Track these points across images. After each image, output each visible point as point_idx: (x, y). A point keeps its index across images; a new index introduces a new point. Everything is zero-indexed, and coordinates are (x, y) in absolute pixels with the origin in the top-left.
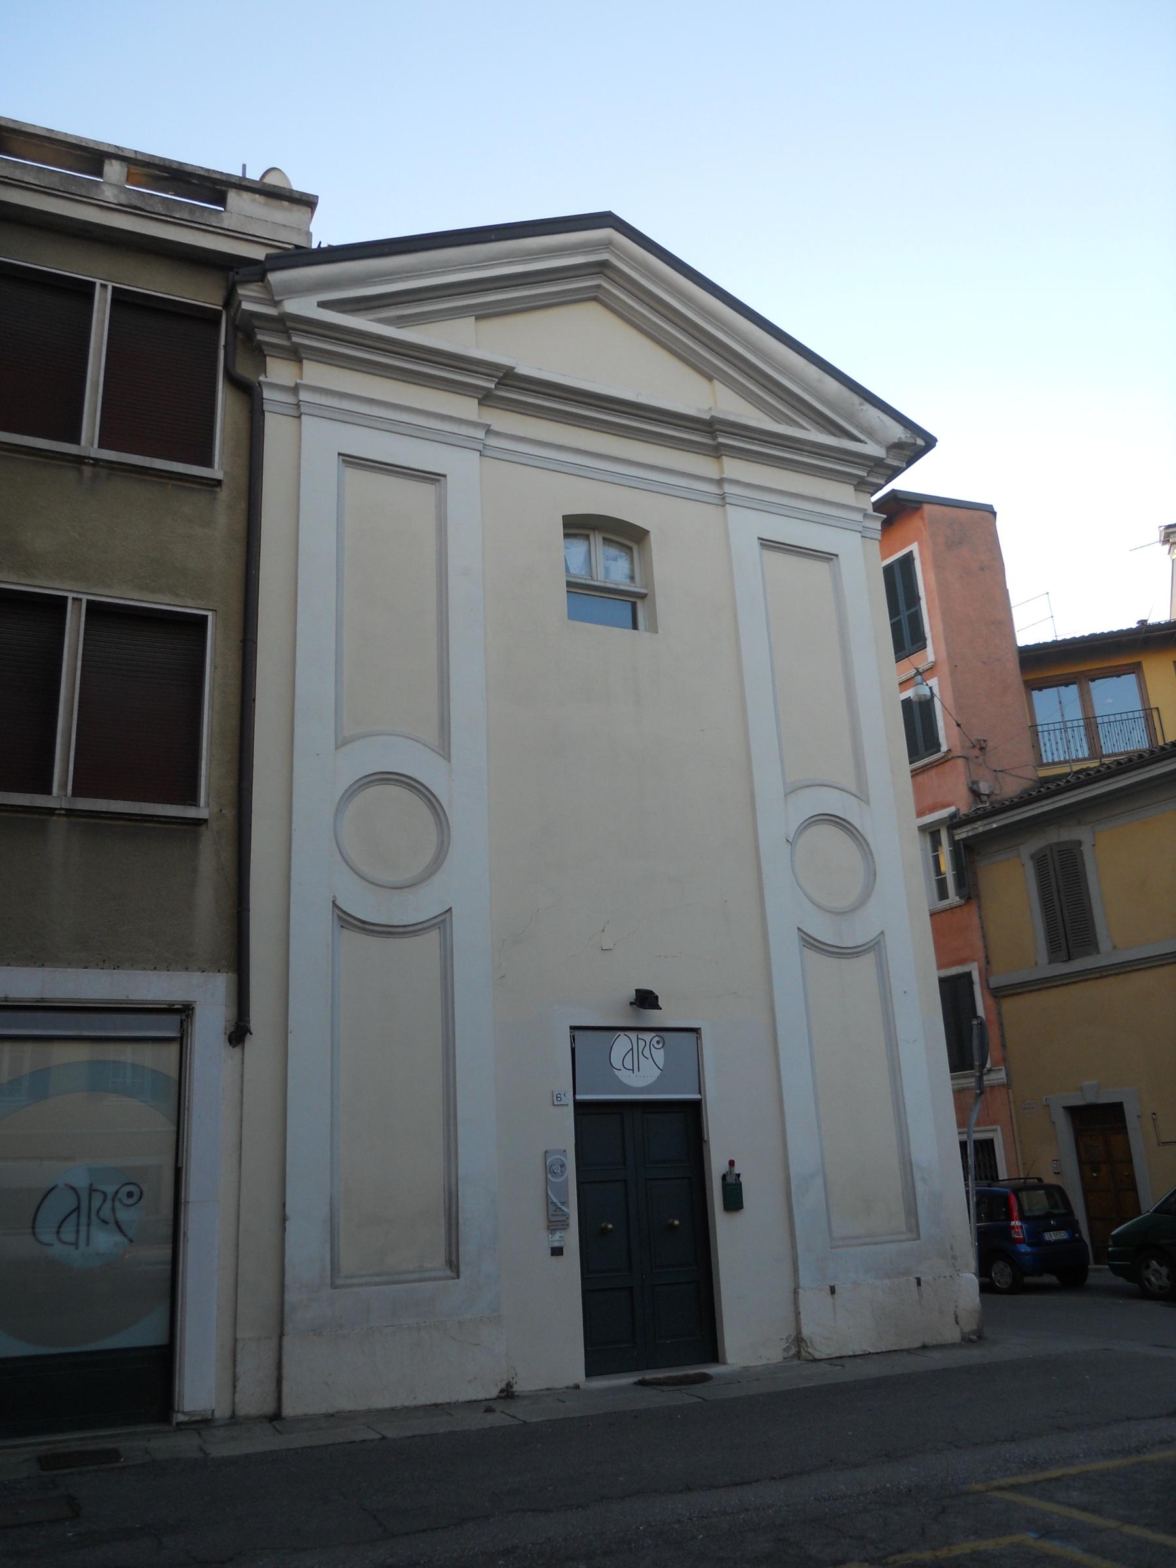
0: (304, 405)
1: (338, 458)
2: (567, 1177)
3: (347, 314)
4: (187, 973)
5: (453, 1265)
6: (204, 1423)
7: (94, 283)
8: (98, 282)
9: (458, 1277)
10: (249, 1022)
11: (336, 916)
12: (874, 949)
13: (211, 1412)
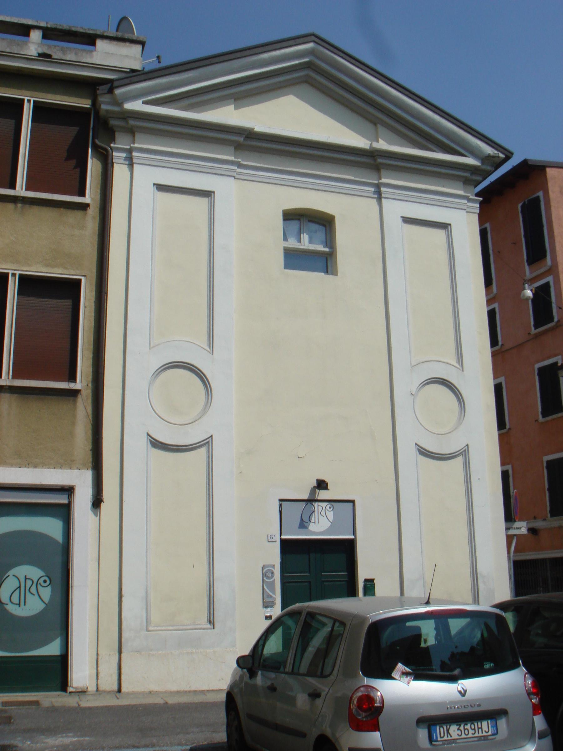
0: (135, 158)
1: (154, 186)
2: (275, 579)
3: (159, 106)
4: (71, 470)
5: (211, 622)
6: (82, 692)
7: (23, 100)
8: (26, 99)
9: (214, 628)
10: (102, 496)
11: (149, 441)
12: (462, 454)
13: (86, 688)
